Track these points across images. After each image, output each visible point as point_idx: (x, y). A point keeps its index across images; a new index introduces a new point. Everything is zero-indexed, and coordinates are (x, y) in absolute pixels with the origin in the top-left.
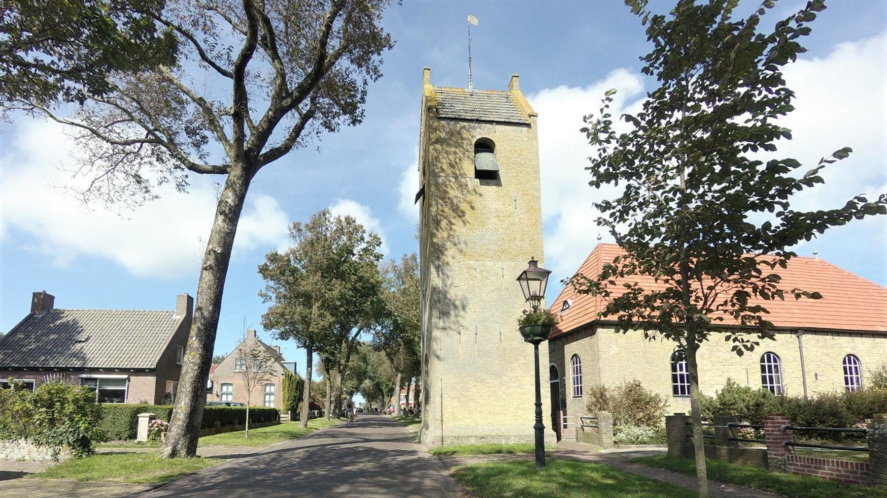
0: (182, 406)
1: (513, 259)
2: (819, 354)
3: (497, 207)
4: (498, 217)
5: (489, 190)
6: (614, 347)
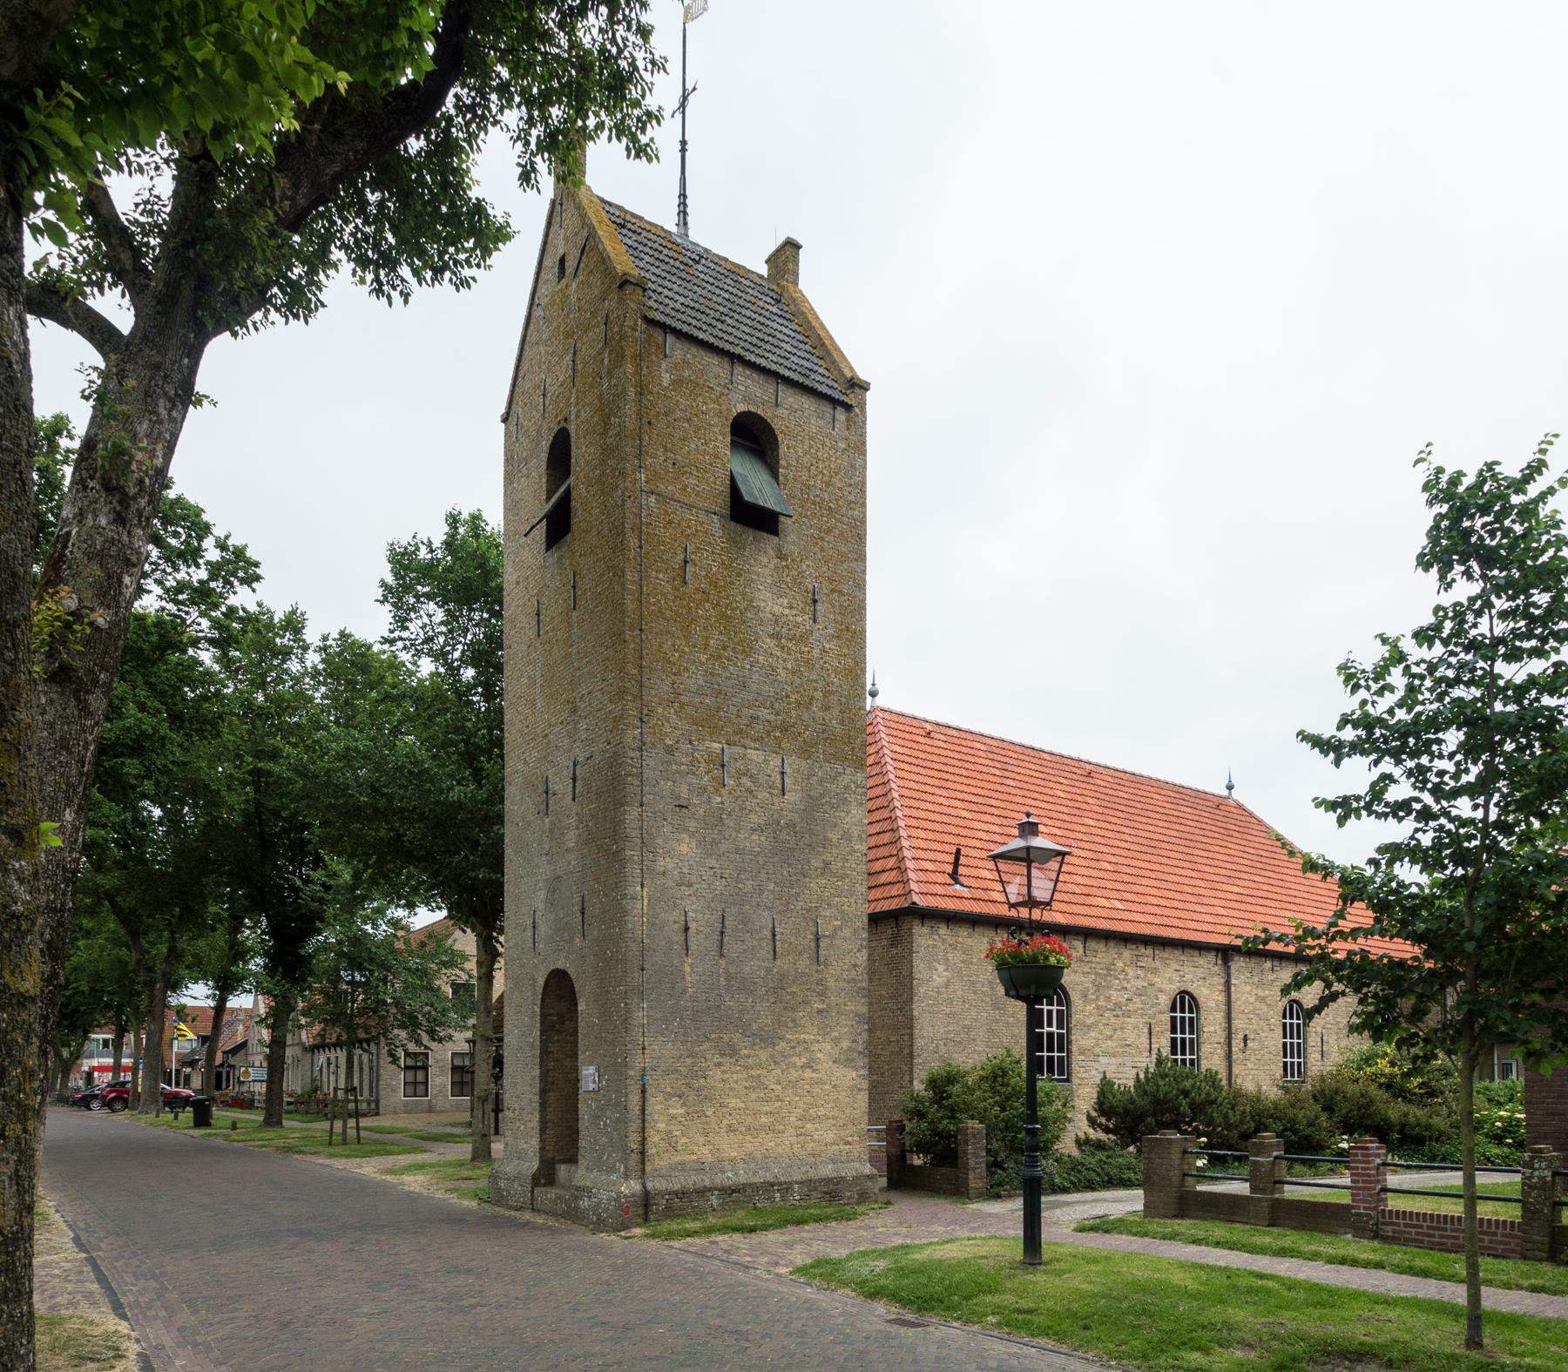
0: (527, 1216)
1: (806, 752)
2: (1252, 1000)
3: (777, 609)
4: (776, 636)
5: (762, 558)
6: (941, 968)
